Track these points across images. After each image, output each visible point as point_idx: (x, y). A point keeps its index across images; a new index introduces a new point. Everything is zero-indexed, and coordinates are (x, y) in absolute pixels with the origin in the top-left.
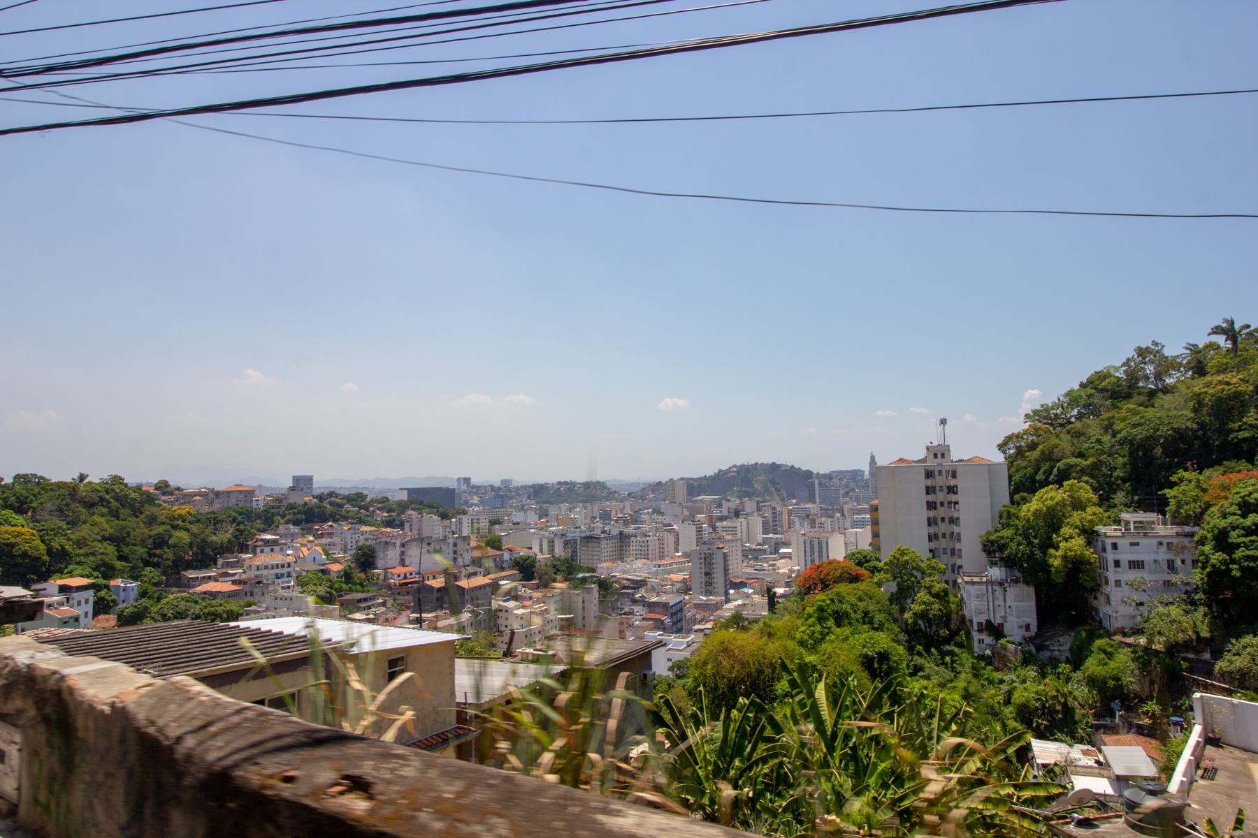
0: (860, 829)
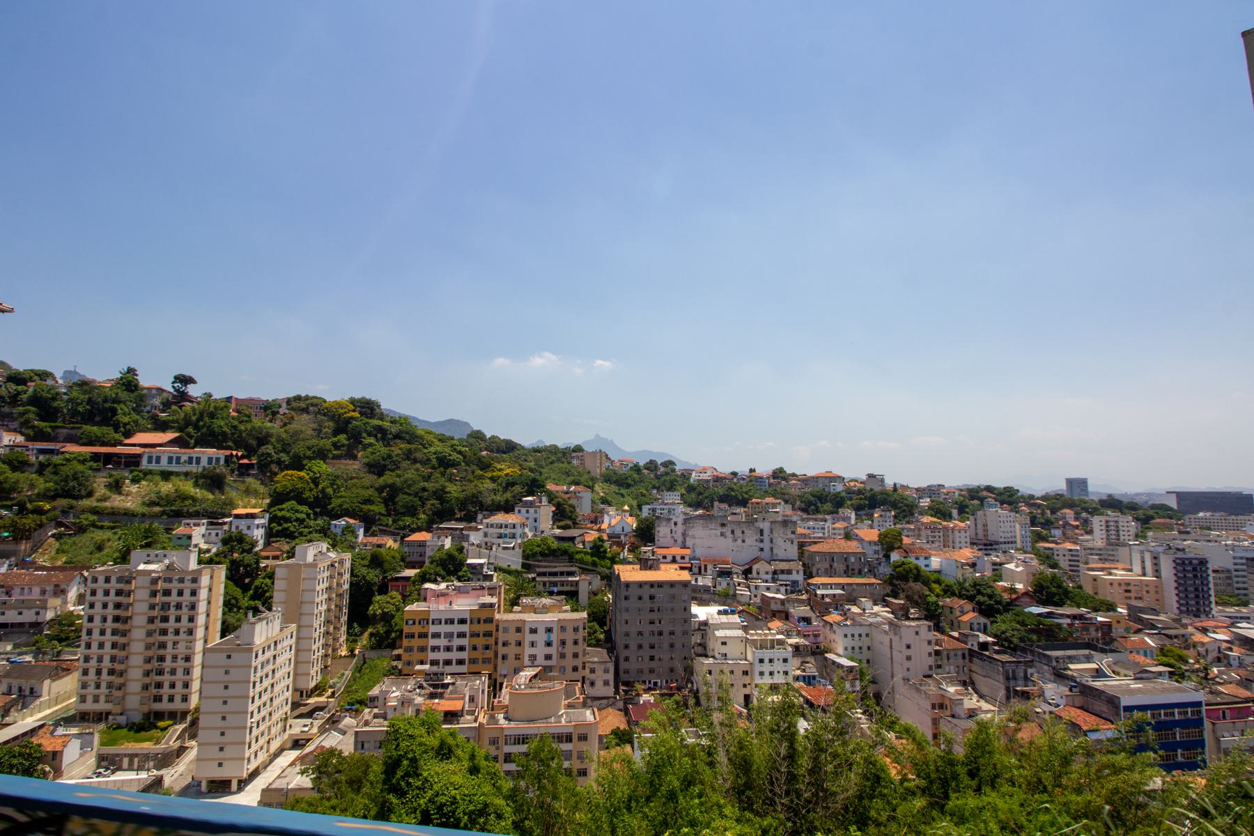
0: (700, 802)
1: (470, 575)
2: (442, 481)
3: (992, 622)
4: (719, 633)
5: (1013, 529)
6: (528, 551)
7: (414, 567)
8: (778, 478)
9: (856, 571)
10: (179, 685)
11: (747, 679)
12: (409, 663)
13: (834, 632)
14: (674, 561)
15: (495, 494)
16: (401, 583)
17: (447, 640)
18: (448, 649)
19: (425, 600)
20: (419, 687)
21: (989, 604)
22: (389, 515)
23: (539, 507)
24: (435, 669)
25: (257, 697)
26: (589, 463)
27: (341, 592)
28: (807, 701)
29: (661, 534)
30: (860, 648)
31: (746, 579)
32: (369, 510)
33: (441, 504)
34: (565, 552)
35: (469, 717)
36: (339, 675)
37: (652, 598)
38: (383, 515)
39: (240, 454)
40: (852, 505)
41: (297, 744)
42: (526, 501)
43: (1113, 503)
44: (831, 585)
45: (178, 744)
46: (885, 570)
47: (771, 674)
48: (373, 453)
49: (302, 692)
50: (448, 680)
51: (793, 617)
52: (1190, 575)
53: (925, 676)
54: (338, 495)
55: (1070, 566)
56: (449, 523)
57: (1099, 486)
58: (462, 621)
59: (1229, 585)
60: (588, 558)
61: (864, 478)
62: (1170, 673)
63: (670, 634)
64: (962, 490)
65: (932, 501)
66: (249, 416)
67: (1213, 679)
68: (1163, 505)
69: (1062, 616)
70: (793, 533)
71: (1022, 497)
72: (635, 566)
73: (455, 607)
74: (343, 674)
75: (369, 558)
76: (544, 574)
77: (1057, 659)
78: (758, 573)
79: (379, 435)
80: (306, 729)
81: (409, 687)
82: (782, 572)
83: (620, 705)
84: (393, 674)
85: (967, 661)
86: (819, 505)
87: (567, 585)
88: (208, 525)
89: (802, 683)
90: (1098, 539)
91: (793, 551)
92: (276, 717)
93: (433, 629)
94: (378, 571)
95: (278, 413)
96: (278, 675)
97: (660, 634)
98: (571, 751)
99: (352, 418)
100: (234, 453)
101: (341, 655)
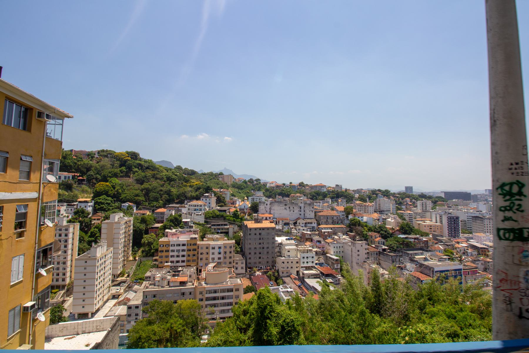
1: (184, 226)
2: (169, 187)
3: (386, 241)
4: (287, 247)
5: (389, 206)
6: (207, 216)
7: (159, 223)
8: (301, 186)
9: (336, 222)
10: (61, 274)
11: (298, 265)
12: (161, 262)
13: (330, 246)
14: (266, 219)
15: (192, 193)
16: (154, 230)
17: (177, 253)
18: (178, 256)
19: (167, 236)
20: (168, 272)
21: (385, 234)
22: (146, 201)
23: (211, 198)
24: (172, 264)
25: (98, 278)
26: (226, 180)
27: (130, 234)
28: (321, 273)
29: (261, 209)
30: (340, 252)
31: (295, 226)
32: (138, 199)
33: (169, 197)
34: (222, 216)
35: (190, 284)
36: (130, 268)
37: (260, 234)
38: (144, 201)
39: (78, 175)
40: (330, 196)
41: (114, 297)
42: (205, 196)
43: (423, 196)
44: (327, 228)
45: (62, 299)
46: (347, 222)
47: (307, 262)
48: (138, 175)
49: (115, 276)
50: (180, 269)
51: (314, 241)
52: (453, 223)
53: (364, 262)
54: (124, 193)
55: (409, 219)
56: (172, 204)
57: (418, 189)
58: (184, 245)
59: (465, 226)
60: (232, 219)
61: (334, 186)
62: (449, 258)
63: (267, 248)
64: (369, 191)
65: (359, 195)
66: (82, 159)
67: (463, 260)
68: (440, 197)
69: (411, 238)
70: (313, 208)
71: (391, 193)
72: (252, 222)
73: (180, 239)
74: (132, 268)
75: (140, 219)
76: (214, 225)
77: (411, 254)
78: (299, 224)
79: (140, 167)
80: (118, 291)
81: (164, 272)
82: (309, 223)
83: (248, 276)
84: (154, 267)
85: (378, 255)
86: (317, 197)
87: (224, 229)
88: (67, 206)
89: (318, 266)
90: (419, 210)
91: (312, 215)
92: (106, 286)
93: (171, 248)
94: (145, 225)
95: (94, 157)
96: (106, 269)
97: (263, 248)
98: (232, 295)
99: (127, 160)
100: (76, 174)
101: (130, 260)
